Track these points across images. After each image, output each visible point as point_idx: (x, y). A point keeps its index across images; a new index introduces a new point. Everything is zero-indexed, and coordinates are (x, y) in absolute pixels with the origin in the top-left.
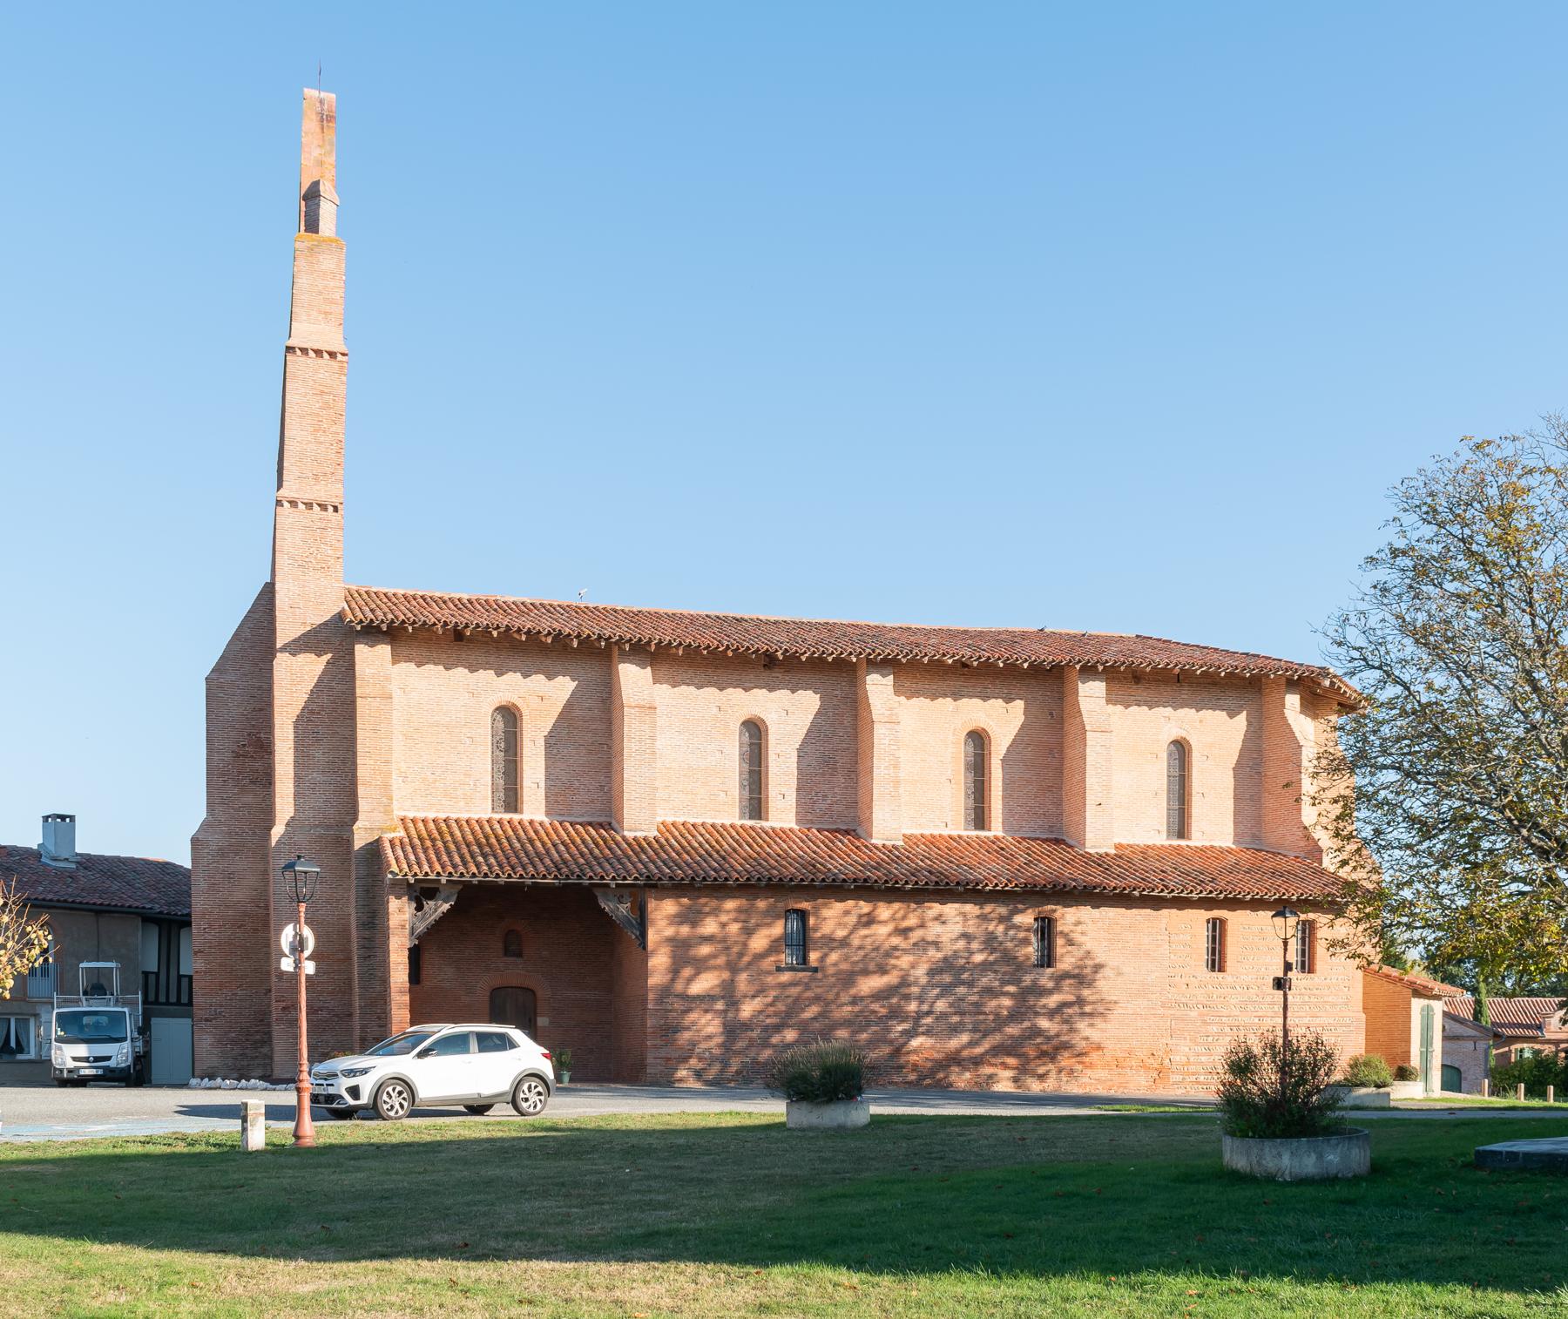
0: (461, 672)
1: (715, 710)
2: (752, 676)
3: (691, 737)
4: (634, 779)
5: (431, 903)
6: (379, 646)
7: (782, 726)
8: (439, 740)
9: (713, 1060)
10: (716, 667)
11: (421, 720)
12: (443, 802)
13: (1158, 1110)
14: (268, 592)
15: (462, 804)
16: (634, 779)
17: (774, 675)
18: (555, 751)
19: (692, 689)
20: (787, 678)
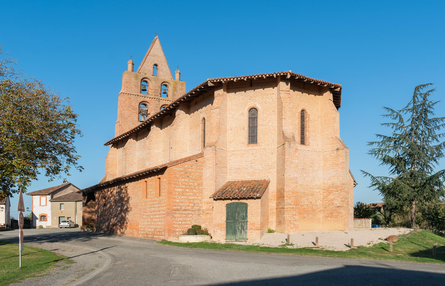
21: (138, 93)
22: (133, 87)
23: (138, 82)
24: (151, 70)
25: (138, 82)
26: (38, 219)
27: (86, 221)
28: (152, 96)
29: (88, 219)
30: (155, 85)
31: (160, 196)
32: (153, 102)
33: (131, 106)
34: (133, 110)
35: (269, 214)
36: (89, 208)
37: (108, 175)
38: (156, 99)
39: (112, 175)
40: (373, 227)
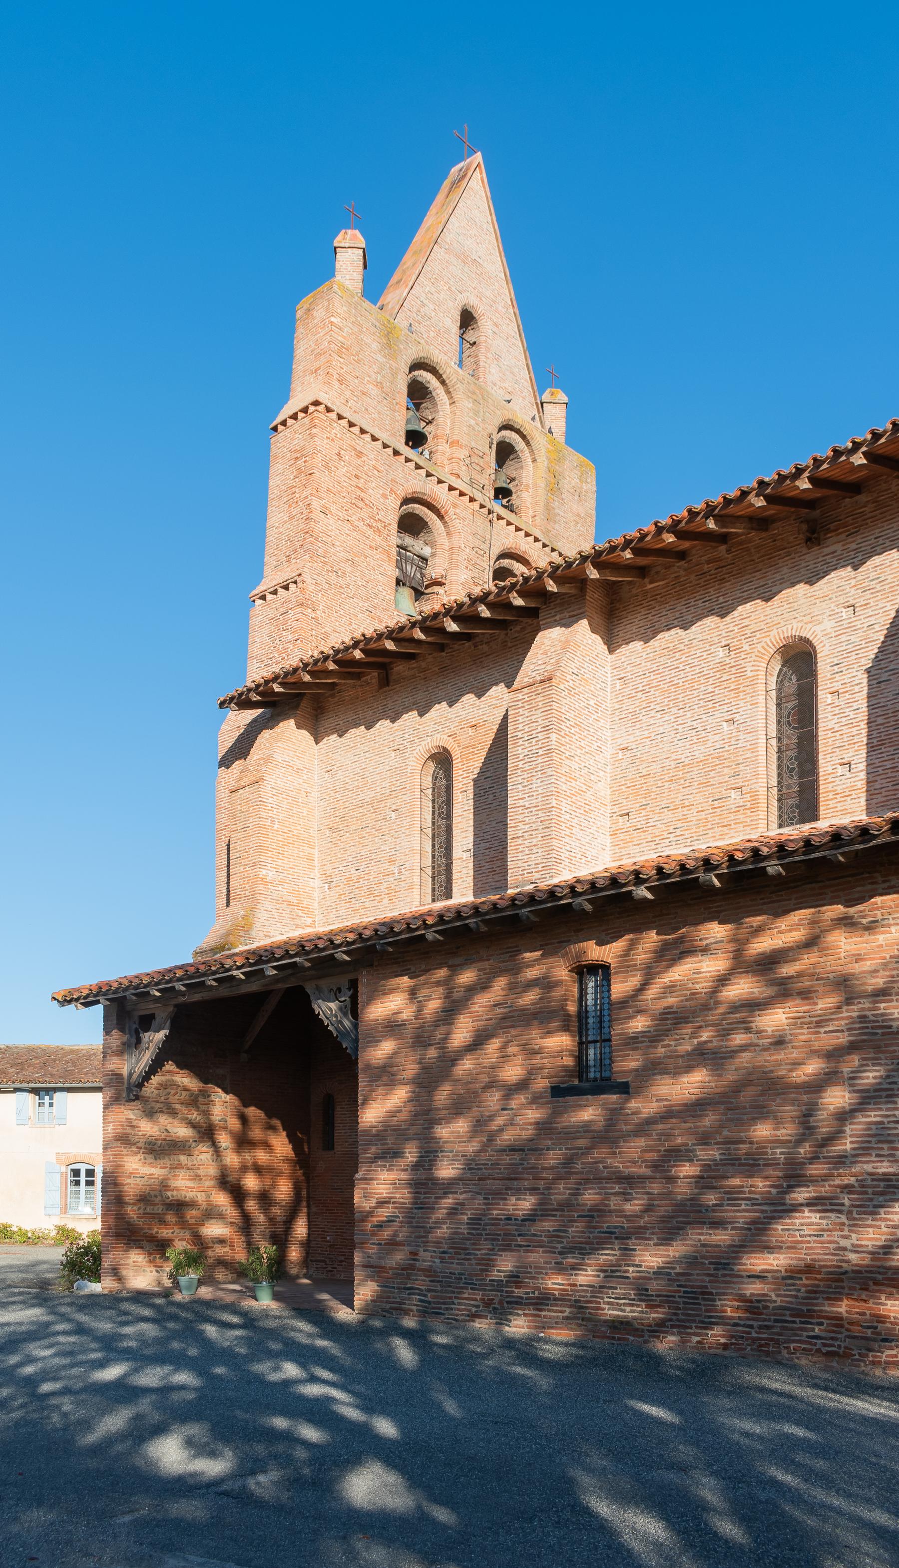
0: (384, 725)
1: (721, 653)
2: (785, 570)
3: (681, 713)
4: (521, 803)
5: (147, 1034)
6: (281, 724)
7: (844, 638)
8: (364, 825)
9: (392, 1244)
10: (722, 580)
11: (347, 804)
12: (367, 904)
13: (830, 1395)
14: (505, 718)
15: (386, 901)
16: (521, 803)
17: (827, 550)
18: (491, 797)
19: (676, 634)
20: (853, 546)
21: (394, 435)
22: (374, 391)
23: (394, 374)
24: (447, 331)
25: (394, 374)
26: (352, 1307)
27: (132, 1212)
28: (459, 481)
29: (144, 1199)
30: (473, 422)
31: (228, 906)
32: (464, 519)
33: (361, 504)
34: (370, 532)
35: (594, 952)
36: (150, 1114)
37: (268, 905)
38: (476, 505)
39: (290, 904)
40: (450, 706)
